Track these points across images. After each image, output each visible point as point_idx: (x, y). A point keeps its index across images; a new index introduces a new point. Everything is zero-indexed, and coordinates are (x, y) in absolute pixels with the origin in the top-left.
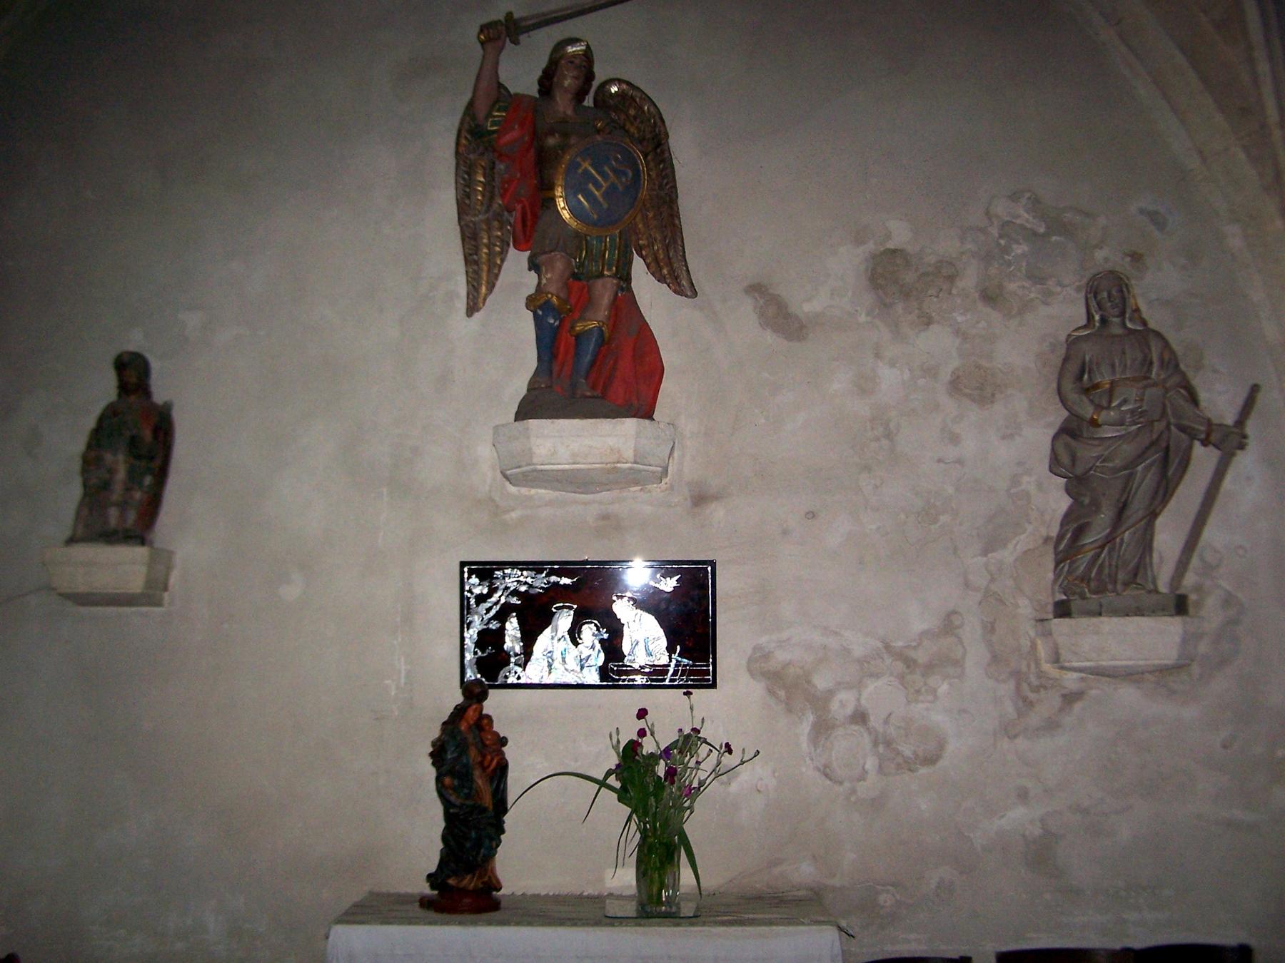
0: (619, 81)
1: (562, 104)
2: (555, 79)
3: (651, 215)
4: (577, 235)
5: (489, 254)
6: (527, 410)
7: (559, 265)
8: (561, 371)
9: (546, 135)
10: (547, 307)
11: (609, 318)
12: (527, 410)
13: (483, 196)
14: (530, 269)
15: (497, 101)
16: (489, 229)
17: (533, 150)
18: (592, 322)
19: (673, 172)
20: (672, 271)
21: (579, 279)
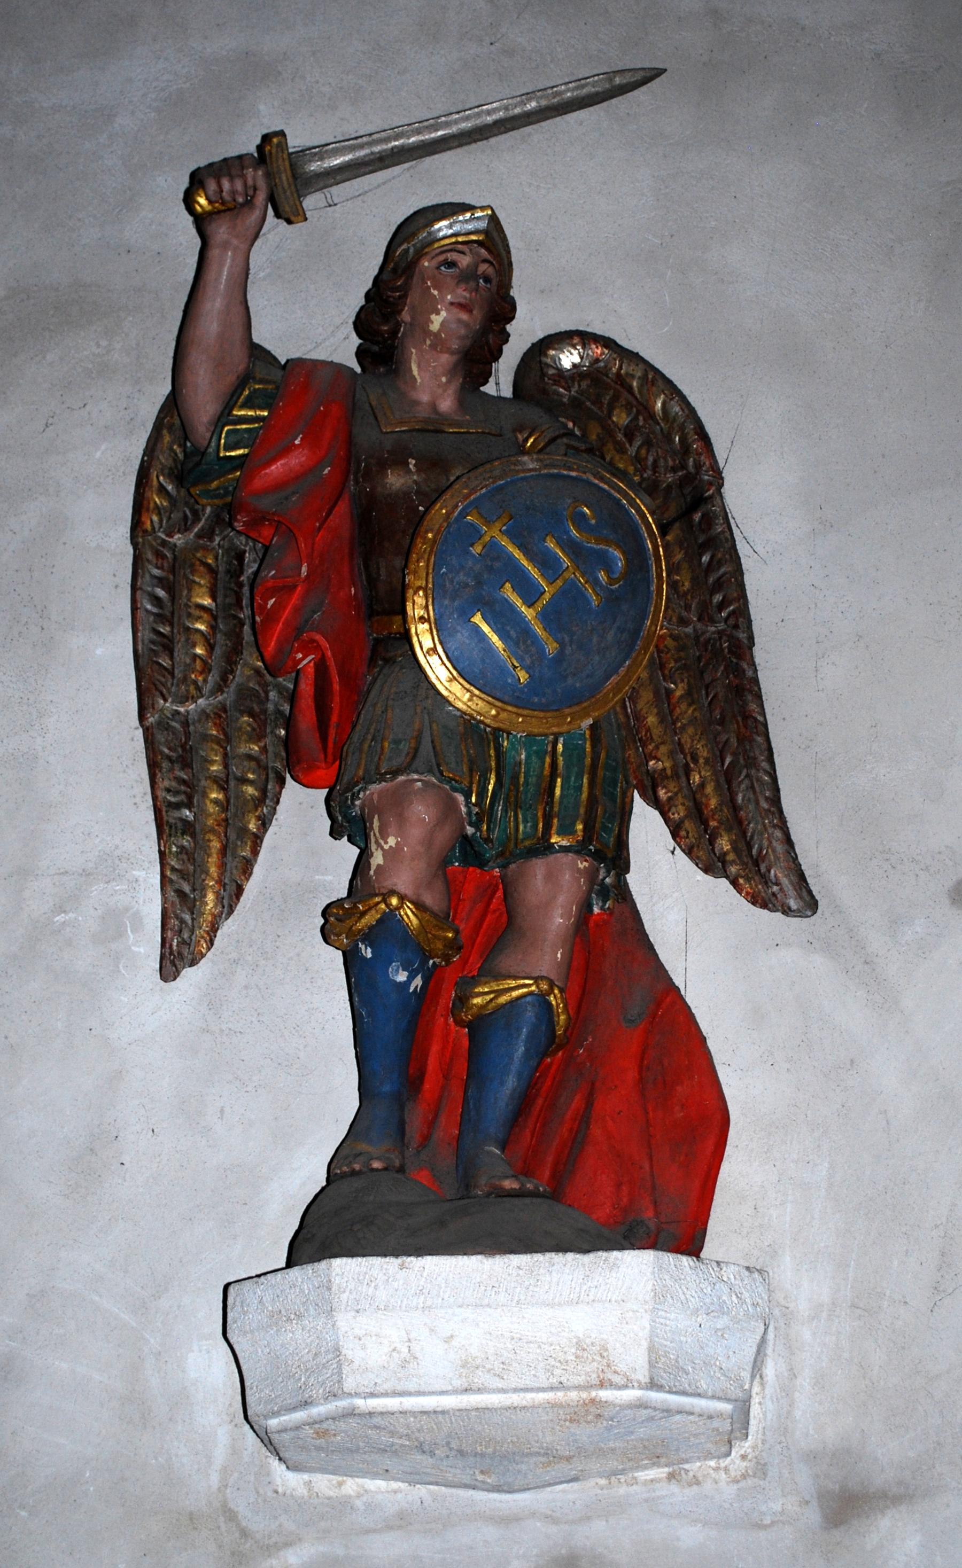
0: (584, 338)
1: (428, 380)
2: (406, 316)
3: (679, 690)
4: (469, 726)
5: (224, 806)
6: (319, 1236)
7: (422, 812)
8: (431, 1124)
9: (383, 465)
10: (387, 931)
11: (569, 965)
12: (319, 1236)
13: (210, 647)
14: (335, 833)
15: (244, 380)
16: (226, 741)
17: (343, 507)
18: (521, 983)
19: (738, 571)
20: (743, 843)
21: (478, 866)
